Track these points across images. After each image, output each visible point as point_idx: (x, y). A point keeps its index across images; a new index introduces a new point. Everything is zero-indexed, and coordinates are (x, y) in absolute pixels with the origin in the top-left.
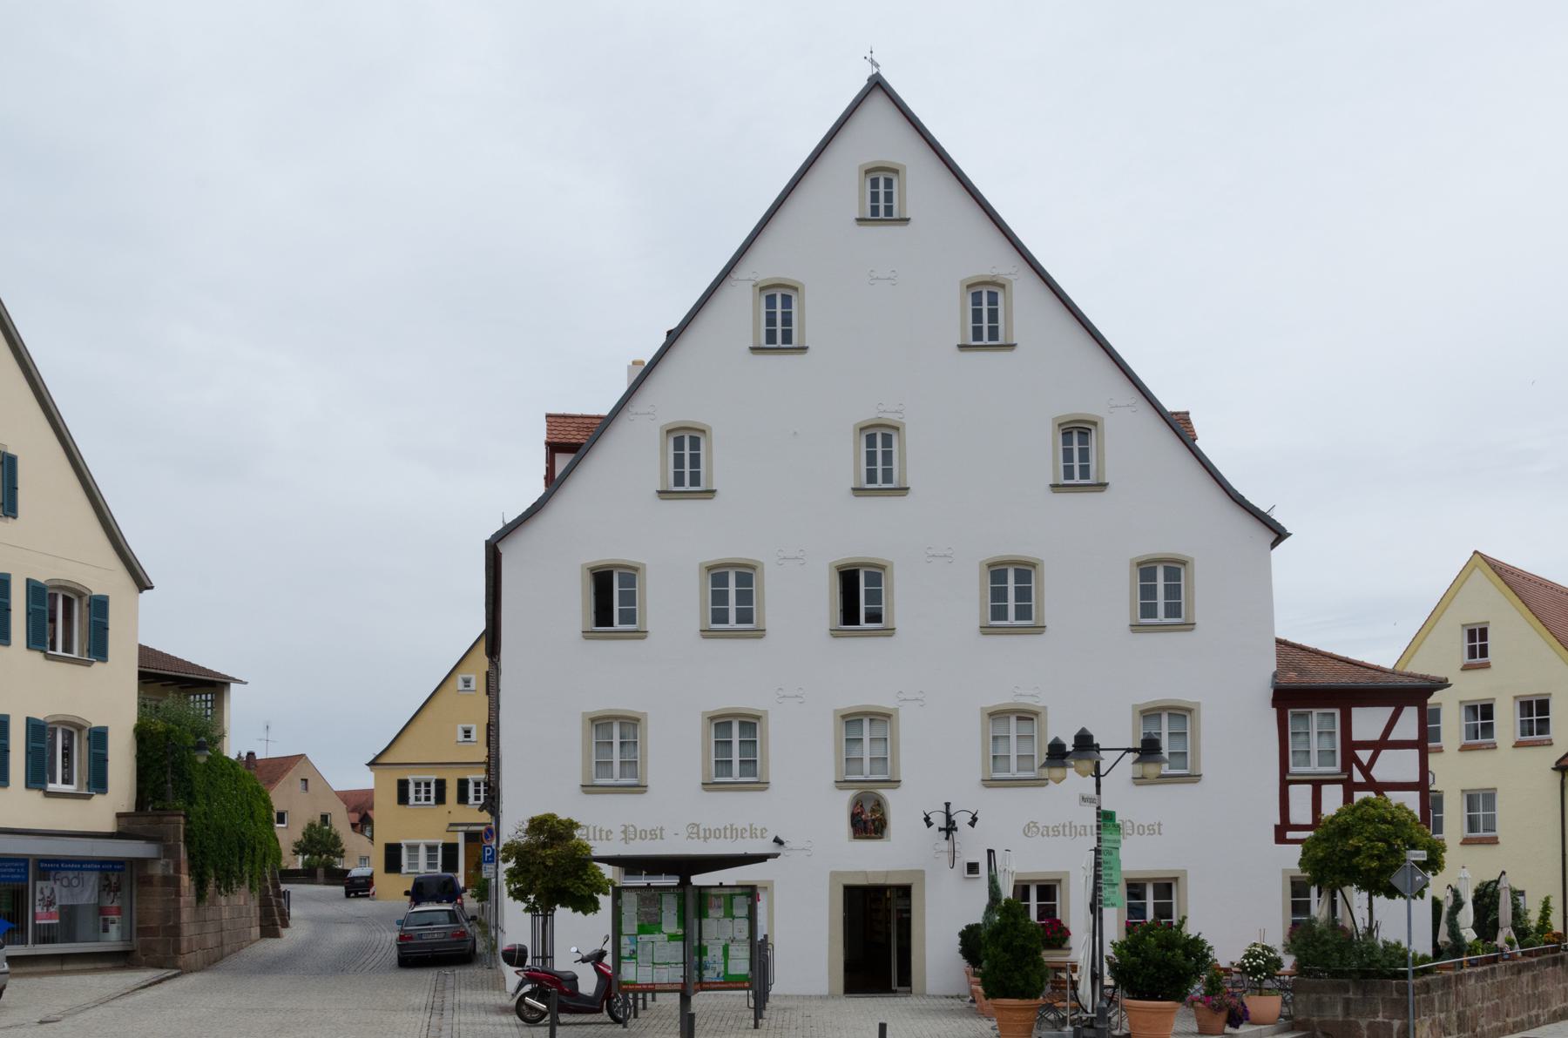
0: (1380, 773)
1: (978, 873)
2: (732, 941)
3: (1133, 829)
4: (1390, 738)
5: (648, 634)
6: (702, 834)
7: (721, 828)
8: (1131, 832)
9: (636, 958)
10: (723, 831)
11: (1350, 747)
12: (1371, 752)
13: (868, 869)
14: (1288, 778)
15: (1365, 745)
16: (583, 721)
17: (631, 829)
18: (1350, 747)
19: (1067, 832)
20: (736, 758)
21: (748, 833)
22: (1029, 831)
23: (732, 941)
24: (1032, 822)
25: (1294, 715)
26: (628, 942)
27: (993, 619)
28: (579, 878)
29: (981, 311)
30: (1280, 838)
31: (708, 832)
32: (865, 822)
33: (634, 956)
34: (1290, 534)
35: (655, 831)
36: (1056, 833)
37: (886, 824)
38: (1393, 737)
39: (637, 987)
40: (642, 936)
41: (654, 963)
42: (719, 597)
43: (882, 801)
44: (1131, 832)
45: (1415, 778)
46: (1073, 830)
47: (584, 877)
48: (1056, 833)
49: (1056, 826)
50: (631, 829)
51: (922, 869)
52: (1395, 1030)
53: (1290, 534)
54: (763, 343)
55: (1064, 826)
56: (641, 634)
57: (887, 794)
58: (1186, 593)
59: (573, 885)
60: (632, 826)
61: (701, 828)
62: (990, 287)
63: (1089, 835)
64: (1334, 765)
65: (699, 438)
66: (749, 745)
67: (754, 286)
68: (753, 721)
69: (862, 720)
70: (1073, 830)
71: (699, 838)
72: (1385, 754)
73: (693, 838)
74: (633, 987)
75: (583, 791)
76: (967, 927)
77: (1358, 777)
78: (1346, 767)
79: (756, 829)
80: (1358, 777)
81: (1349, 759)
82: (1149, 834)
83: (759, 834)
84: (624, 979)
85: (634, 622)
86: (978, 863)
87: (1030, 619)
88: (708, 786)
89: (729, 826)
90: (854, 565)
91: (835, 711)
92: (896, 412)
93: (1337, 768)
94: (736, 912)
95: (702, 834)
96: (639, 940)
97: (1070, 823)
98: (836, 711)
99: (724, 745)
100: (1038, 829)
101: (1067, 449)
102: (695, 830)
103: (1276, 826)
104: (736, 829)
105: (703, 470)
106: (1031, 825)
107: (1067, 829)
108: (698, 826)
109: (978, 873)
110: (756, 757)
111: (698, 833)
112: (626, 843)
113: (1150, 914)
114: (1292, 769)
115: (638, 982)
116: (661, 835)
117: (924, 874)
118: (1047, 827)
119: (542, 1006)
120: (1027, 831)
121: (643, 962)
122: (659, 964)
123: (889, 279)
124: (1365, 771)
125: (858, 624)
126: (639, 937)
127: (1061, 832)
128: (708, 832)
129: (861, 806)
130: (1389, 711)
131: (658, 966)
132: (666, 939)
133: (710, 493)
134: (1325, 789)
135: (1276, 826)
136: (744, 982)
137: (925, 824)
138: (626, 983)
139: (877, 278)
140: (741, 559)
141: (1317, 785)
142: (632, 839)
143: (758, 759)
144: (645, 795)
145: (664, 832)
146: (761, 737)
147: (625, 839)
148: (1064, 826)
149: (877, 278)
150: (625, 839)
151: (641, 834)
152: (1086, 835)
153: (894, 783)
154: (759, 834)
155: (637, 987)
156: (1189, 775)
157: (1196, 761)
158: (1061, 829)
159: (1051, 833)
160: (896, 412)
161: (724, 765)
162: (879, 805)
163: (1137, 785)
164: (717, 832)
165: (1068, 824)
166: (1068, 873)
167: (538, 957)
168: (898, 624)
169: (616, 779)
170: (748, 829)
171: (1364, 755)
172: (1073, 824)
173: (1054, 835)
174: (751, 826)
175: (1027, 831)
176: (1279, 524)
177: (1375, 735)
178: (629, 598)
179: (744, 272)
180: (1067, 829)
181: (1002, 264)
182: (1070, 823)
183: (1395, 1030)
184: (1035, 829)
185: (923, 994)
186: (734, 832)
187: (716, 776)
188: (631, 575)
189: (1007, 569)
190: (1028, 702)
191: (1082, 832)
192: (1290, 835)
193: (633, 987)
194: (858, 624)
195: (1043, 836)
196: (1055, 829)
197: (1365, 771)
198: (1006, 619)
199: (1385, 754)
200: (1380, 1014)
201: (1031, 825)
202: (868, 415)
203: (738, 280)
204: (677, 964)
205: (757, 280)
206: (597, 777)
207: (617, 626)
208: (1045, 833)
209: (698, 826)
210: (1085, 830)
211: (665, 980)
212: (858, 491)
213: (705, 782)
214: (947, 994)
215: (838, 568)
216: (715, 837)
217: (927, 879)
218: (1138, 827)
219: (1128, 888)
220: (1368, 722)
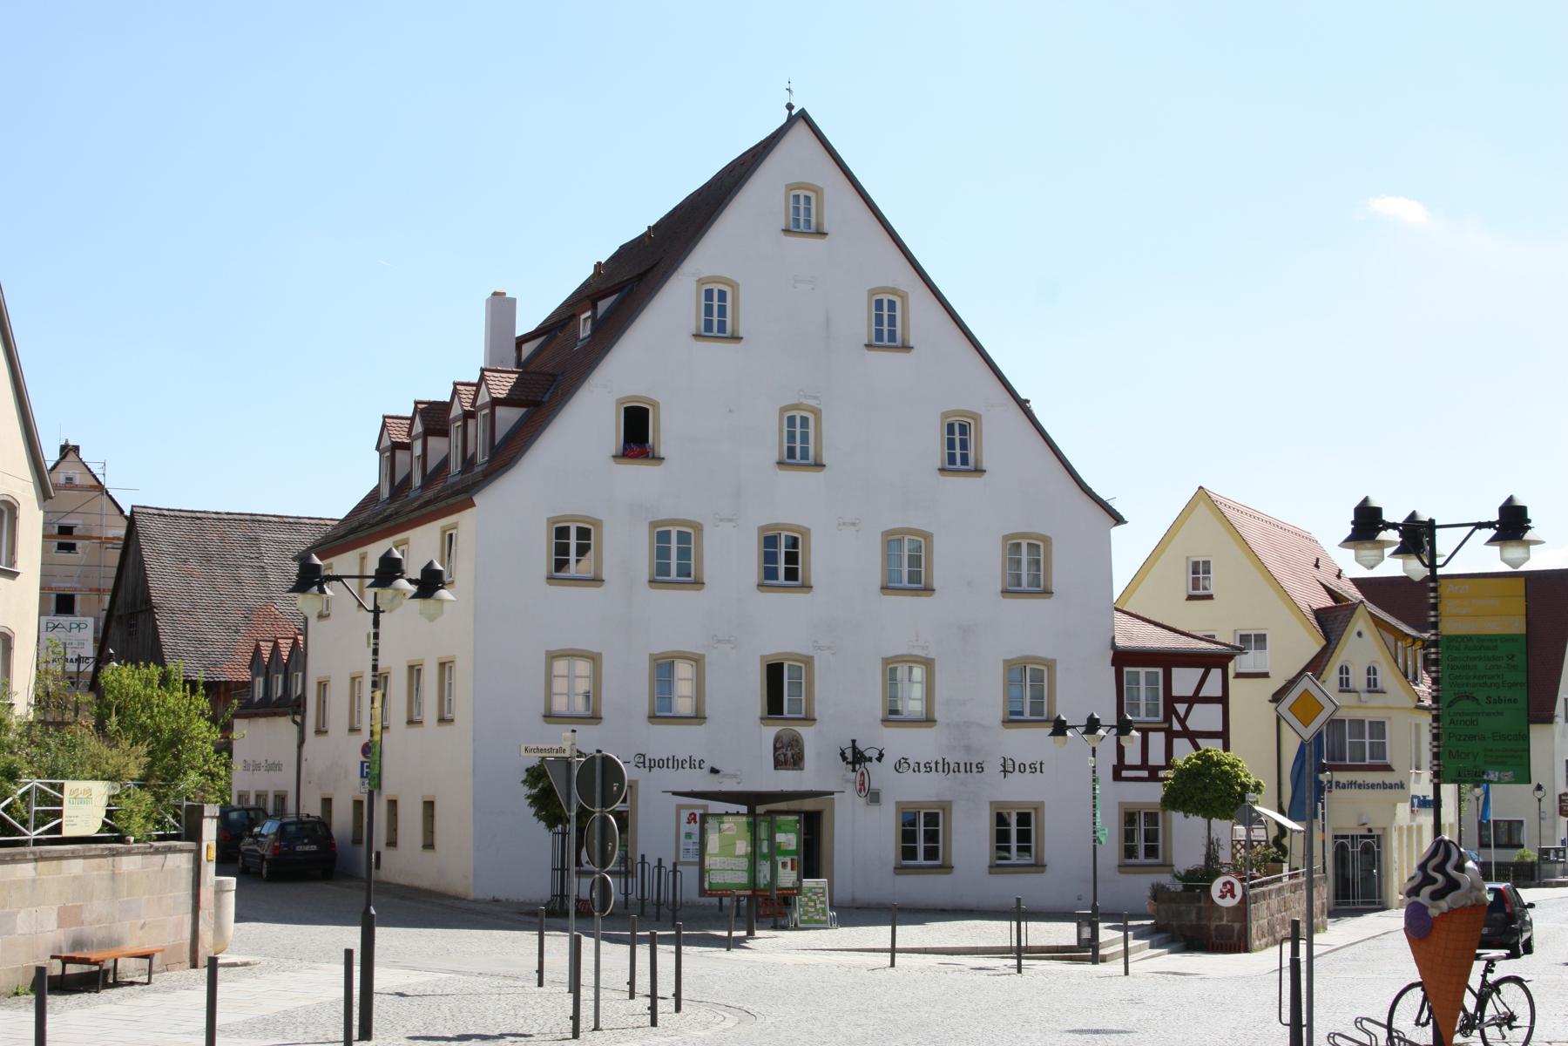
0: (1193, 724)
3: (1014, 767)
4: (1201, 695)
6: (647, 764)
7: (665, 759)
8: (1012, 770)
11: (1170, 701)
12: (1186, 705)
15: (1182, 700)
18: (1170, 701)
21: (688, 764)
31: (653, 762)
34: (1126, 522)
38: (1202, 694)
44: (1012, 770)
45: (1219, 728)
46: (946, 766)
48: (1033, 770)
49: (928, 763)
52: (1236, 931)
53: (1126, 522)
55: (937, 763)
58: (695, 552)
60: (1011, 759)
63: (941, 772)
64: (1158, 716)
70: (946, 766)
71: (645, 767)
72: (1197, 707)
73: (639, 767)
77: (1176, 726)
78: (1167, 719)
80: (1176, 726)
81: (1170, 711)
83: (697, 766)
93: (1161, 718)
95: (647, 764)
97: (674, 757)
102: (642, 760)
104: (678, 760)
108: (644, 756)
111: (644, 763)
120: (898, 767)
124: (1182, 722)
128: (653, 762)
130: (1201, 671)
134: (1151, 735)
137: (840, 758)
141: (1145, 733)
145: (1043, 766)
165: (941, 762)
167: (558, 869)
170: (688, 760)
171: (1181, 708)
172: (676, 758)
175: (898, 767)
177: (1190, 693)
182: (674, 757)
183: (1236, 931)
184: (906, 765)
191: (956, 769)
192: (1125, 774)
195: (914, 771)
197: (1182, 722)
198: (777, 579)
199: (1198, 708)
200: (1225, 919)
201: (902, 761)
208: (916, 769)
212: (942, 470)
219: (1510, 823)
220: (1184, 680)
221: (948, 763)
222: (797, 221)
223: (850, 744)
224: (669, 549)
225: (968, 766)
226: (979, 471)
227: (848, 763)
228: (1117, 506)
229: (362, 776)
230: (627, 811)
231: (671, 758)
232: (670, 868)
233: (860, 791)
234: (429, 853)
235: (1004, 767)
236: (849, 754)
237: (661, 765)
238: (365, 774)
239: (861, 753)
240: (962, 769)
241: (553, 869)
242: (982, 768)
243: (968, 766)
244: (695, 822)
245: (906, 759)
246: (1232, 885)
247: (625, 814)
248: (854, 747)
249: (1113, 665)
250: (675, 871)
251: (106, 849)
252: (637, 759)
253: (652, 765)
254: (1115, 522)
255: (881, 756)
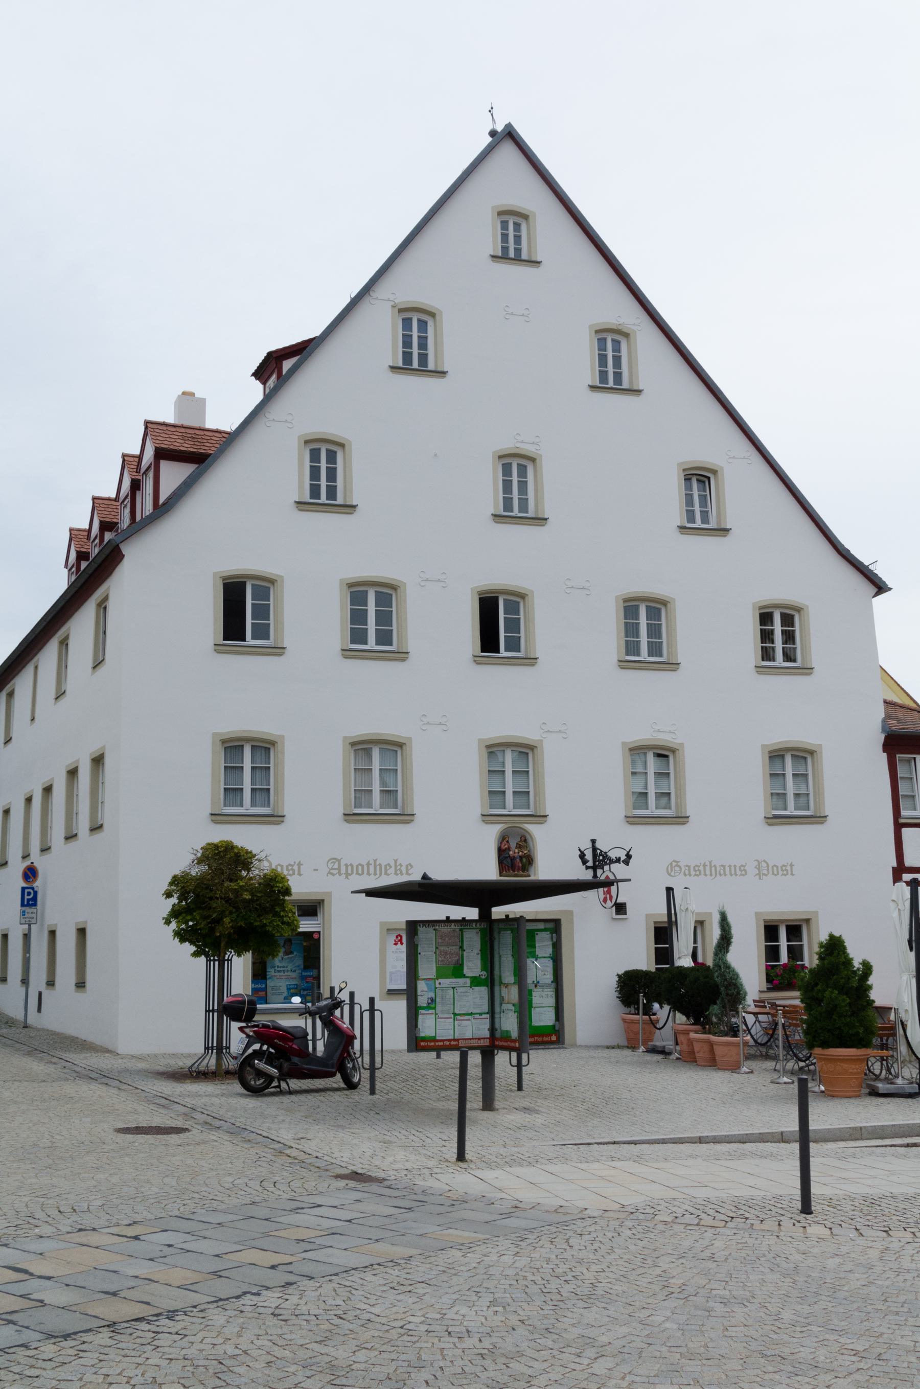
1: (625, 914)
2: (536, 986)
5: (286, 651)
6: (343, 870)
7: (364, 863)
9: (435, 1008)
10: (366, 867)
13: (516, 911)
14: (901, 821)
16: (213, 743)
17: (764, 864)
19: (708, 872)
20: (247, 786)
21: (393, 869)
22: (672, 871)
23: (536, 986)
24: (674, 861)
25: (901, 760)
26: (426, 989)
27: (353, 642)
28: (277, 914)
29: (606, 356)
30: (897, 878)
31: (350, 868)
32: (513, 859)
33: (433, 1006)
34: (890, 589)
35: (786, 866)
36: (698, 873)
37: (532, 860)
39: (437, 1044)
40: (440, 980)
41: (455, 1014)
42: (358, 617)
43: (528, 837)
47: (282, 914)
50: (764, 864)
51: (570, 909)
53: (890, 589)
54: (400, 364)
55: (705, 866)
56: (278, 650)
57: (535, 830)
59: (271, 922)
61: (343, 863)
62: (614, 335)
65: (335, 452)
66: (262, 771)
67: (393, 307)
68: (267, 746)
69: (242, 746)
71: (340, 874)
74: (432, 1044)
75: (212, 820)
76: (871, 966)
79: (401, 865)
82: (782, 875)
84: (422, 1035)
85: (267, 638)
86: (625, 904)
87: (391, 644)
88: (349, 817)
89: (708, 863)
90: (491, 591)
91: (214, 734)
92: (533, 443)
94: (539, 952)
95: (343, 870)
96: (437, 985)
98: (345, 738)
99: (233, 771)
100: (680, 867)
101: (507, 480)
102: (336, 866)
103: (893, 868)
104: (380, 865)
105: (340, 483)
106: (674, 864)
107: (708, 868)
108: (339, 861)
109: (625, 914)
110: (269, 785)
111: (339, 869)
112: (760, 879)
113: (784, 958)
114: (904, 813)
115: (437, 1038)
116: (792, 871)
117: (572, 916)
118: (689, 867)
119: (274, 1071)
121: (442, 1012)
122: (460, 1015)
123: (523, 315)
125: (498, 652)
126: (437, 982)
127: (296, 872)
128: (350, 868)
129: (508, 842)
131: (459, 1017)
132: (469, 984)
133: (350, 508)
135: (893, 868)
136: (551, 1035)
138: (424, 1039)
139: (512, 314)
140: (382, 577)
142: (766, 875)
143: (272, 787)
144: (283, 825)
146: (675, 770)
147: (759, 874)
148: (705, 866)
149: (512, 314)
150: (759, 874)
151: (773, 869)
152: (725, 875)
153: (541, 818)
154: (404, 871)
155: (437, 1044)
156: (812, 817)
157: (819, 802)
158: (701, 868)
159: (693, 873)
160: (533, 443)
161: (233, 793)
162: (524, 841)
163: (770, 825)
164: (360, 868)
166: (816, 913)
168: (815, 662)
169: (247, 807)
170: (392, 864)
173: (741, 875)
174: (396, 861)
175: (670, 871)
176: (880, 579)
178: (262, 612)
179: (383, 291)
180: (708, 868)
181: (631, 317)
184: (677, 869)
185: (574, 1045)
186: (378, 868)
187: (355, 807)
188: (517, 599)
189: (367, 591)
190: (665, 738)
191: (722, 872)
193: (432, 1044)
194: (498, 652)
195: (685, 875)
196: (290, 868)
201: (674, 864)
202: (507, 444)
203: (377, 299)
204: (481, 1014)
205: (396, 301)
206: (225, 806)
207: (503, 652)
208: (687, 872)
209: (339, 861)
210: (724, 869)
211: (468, 1035)
212: (301, 505)
213: (346, 813)
214: (608, 1044)
215: (224, 579)
216: (357, 873)
217: (576, 920)
218: (773, 867)
221: (715, 866)
222: (517, 226)
223: (590, 845)
224: (377, 604)
225: (733, 868)
226: (350, 508)
227: (587, 868)
228: (880, 571)
229: (23, 905)
230: (319, 932)
231: (372, 862)
232: (366, 1006)
233: (605, 900)
234: (80, 996)
235: (759, 869)
236: (589, 856)
237: (360, 872)
238: (26, 903)
239: (605, 855)
240: (727, 872)
241: (208, 1011)
242: (745, 871)
243: (733, 868)
244: (402, 944)
245: (677, 862)
246: (401, 937)
247: (316, 936)
248: (594, 849)
249: (884, 751)
250: (372, 1010)
251: (603, 1138)
252: (330, 866)
253: (350, 871)
254: (876, 590)
255: (629, 856)
